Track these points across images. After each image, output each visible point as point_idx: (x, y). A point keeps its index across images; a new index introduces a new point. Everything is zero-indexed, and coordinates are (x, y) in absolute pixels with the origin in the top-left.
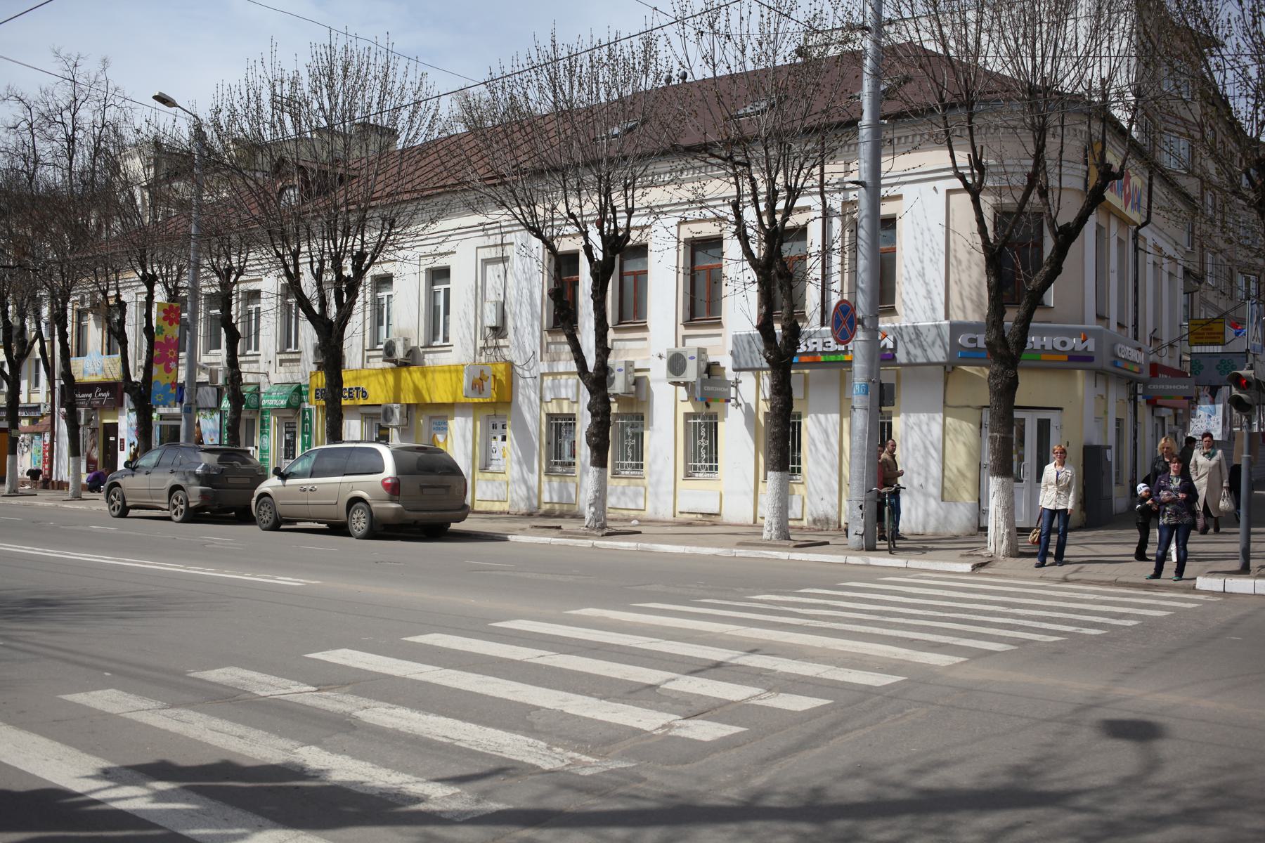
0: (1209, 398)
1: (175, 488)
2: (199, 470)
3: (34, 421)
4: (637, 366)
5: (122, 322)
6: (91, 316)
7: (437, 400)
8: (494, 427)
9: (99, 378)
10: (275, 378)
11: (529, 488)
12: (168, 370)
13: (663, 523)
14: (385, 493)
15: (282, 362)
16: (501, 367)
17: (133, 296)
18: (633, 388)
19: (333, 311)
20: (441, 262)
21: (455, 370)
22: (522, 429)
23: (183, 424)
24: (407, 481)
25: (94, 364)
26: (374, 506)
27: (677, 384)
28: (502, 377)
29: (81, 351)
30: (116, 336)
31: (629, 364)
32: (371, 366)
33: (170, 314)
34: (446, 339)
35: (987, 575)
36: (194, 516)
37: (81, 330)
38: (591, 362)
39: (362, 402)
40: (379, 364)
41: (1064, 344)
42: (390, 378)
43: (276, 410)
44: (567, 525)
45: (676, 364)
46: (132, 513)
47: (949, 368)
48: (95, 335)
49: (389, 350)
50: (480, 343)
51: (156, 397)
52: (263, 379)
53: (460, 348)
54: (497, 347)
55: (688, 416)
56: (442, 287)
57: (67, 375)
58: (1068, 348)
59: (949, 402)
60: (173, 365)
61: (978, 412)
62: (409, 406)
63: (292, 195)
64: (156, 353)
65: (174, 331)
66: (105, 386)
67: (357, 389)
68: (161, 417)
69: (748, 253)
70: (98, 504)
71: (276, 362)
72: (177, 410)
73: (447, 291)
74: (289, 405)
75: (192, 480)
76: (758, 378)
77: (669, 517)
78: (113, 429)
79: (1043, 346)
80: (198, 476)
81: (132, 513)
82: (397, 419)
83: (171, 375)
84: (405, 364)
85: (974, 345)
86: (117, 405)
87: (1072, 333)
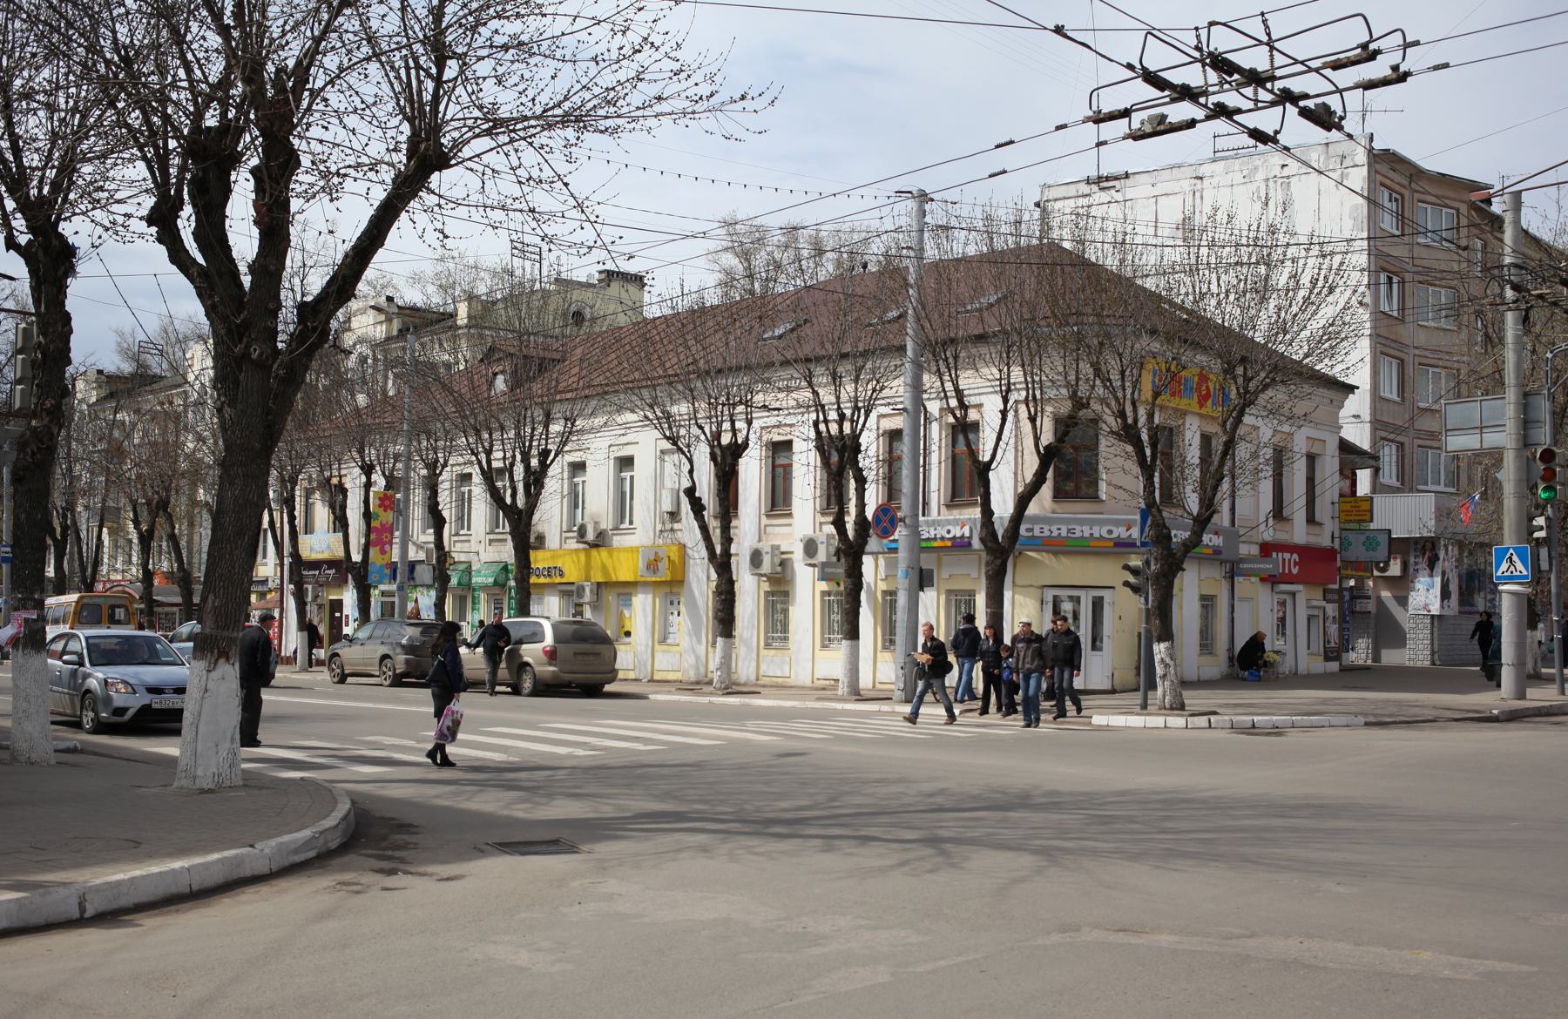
0: (1428, 571)
1: (385, 657)
2: (404, 641)
3: (262, 595)
4: (783, 549)
5: (344, 507)
6: (317, 495)
7: (622, 578)
9: (325, 556)
10: (485, 557)
11: (697, 658)
12: (383, 552)
13: (803, 688)
14: (545, 659)
15: (491, 541)
16: (675, 548)
17: (353, 479)
18: (779, 569)
19: (521, 502)
21: (634, 550)
22: (693, 605)
23: (396, 600)
24: (561, 648)
25: (320, 543)
26: (537, 669)
28: (674, 556)
29: (309, 529)
30: (340, 522)
31: (775, 548)
32: (565, 546)
33: (386, 501)
34: (631, 523)
36: (398, 681)
37: (308, 508)
38: (718, 549)
39: (558, 580)
40: (573, 544)
41: (1110, 532)
42: (582, 557)
43: (484, 588)
46: (349, 680)
48: (322, 514)
49: (582, 532)
50: (659, 527)
51: (372, 578)
52: (474, 558)
53: (641, 533)
54: (672, 530)
55: (824, 593)
57: (295, 554)
58: (1115, 535)
59: (1018, 582)
60: (387, 547)
62: (599, 584)
63: (500, 383)
64: (373, 536)
65: (388, 517)
66: (331, 563)
68: (383, 594)
70: (323, 676)
71: (481, 545)
72: (394, 587)
74: (496, 583)
75: (399, 650)
76: (876, 560)
77: (808, 683)
78: (337, 605)
80: (403, 647)
81: (349, 680)
82: (587, 597)
83: (386, 557)
84: (595, 545)
86: (341, 583)
87: (1117, 523)
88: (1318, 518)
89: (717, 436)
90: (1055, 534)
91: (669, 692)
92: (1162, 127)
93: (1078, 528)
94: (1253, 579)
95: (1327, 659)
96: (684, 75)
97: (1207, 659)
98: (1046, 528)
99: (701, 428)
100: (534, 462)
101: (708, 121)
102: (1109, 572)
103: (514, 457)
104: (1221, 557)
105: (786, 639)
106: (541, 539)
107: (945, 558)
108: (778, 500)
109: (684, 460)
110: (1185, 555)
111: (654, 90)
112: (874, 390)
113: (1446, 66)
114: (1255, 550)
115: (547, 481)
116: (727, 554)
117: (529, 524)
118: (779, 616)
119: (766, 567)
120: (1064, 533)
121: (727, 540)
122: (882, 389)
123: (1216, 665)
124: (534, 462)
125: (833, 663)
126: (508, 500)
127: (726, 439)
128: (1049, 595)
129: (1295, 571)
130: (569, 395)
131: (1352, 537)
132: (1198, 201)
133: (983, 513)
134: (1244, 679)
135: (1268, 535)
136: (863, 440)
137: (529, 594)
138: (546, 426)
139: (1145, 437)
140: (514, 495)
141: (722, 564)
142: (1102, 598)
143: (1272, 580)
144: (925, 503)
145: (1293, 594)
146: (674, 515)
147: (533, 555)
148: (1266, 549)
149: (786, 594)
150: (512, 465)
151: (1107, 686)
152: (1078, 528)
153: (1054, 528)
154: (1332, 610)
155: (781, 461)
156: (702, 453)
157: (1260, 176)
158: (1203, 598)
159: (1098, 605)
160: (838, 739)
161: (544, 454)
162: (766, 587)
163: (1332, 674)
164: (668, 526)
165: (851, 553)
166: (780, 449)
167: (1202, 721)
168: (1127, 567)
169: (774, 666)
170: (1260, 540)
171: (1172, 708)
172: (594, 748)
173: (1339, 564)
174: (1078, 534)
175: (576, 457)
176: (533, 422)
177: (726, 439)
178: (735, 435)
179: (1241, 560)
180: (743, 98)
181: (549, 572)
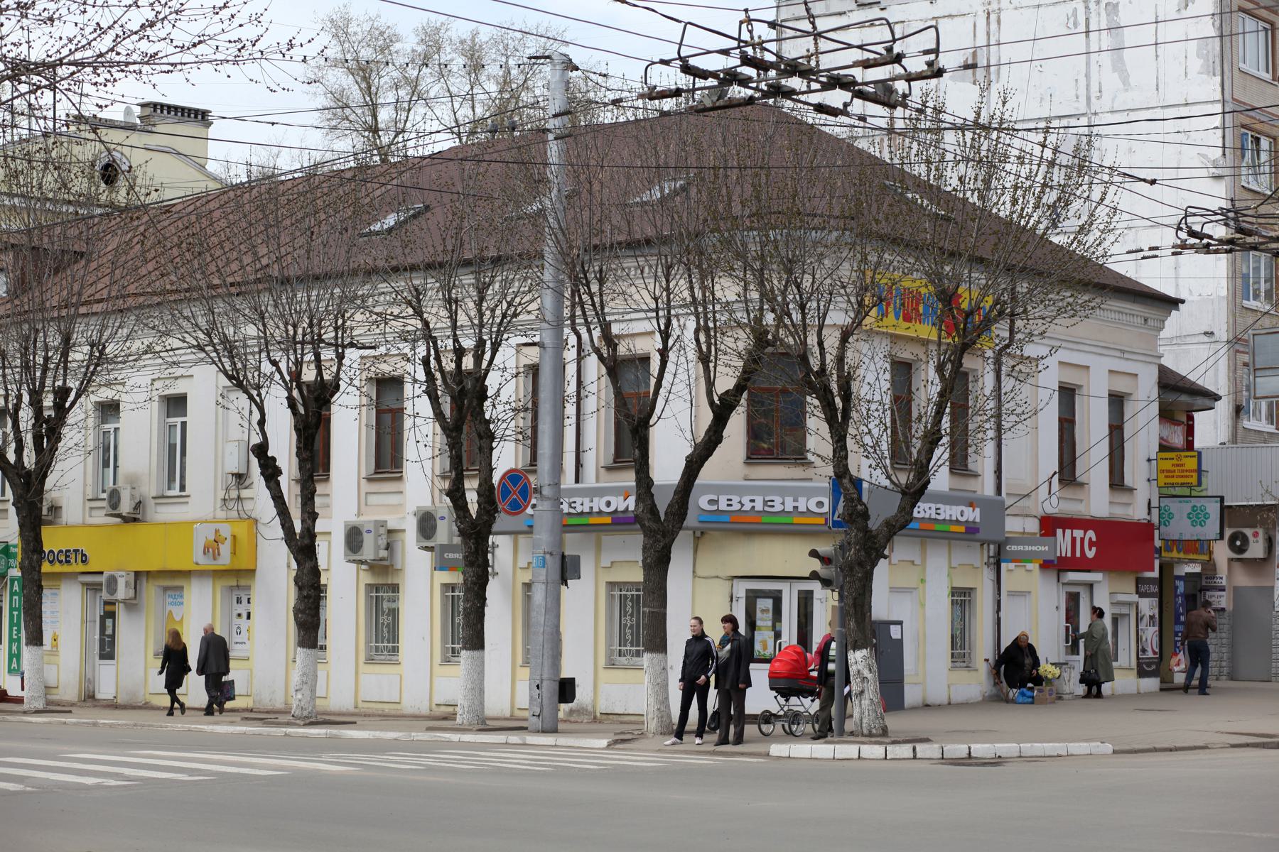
8: (239, 601)
18: (383, 554)
19: (29, 459)
20: (178, 388)
27: (426, 548)
34: (183, 488)
35: (639, 750)
38: (298, 527)
40: (100, 518)
44: (282, 718)
45: (354, 538)
47: (698, 534)
56: (179, 420)
59: (699, 572)
61: (728, 583)
67: (76, 551)
69: (439, 415)
73: (184, 424)
79: (796, 508)
85: (715, 508)
88: (1128, 481)
89: (296, 376)
90: (747, 507)
91: (232, 723)
92: (721, 103)
93: (778, 500)
94: (1029, 566)
95: (1142, 673)
96: (225, 14)
97: (962, 675)
98: (735, 499)
99: (274, 363)
100: (48, 401)
101: (251, 69)
102: (793, 558)
103: (19, 397)
104: (978, 536)
105: (395, 650)
106: (55, 509)
107: (606, 539)
108: (387, 459)
109: (254, 408)
110: (889, 538)
111: (196, 28)
112: (504, 316)
114: (1033, 526)
115: (65, 430)
116: (310, 534)
117: (40, 491)
118: (385, 620)
119: (368, 552)
120: (759, 506)
121: (310, 515)
122: (515, 315)
123: (977, 682)
124: (48, 401)
125: (451, 685)
126: (11, 457)
127: (309, 375)
128: (741, 589)
129: (1091, 554)
130: (97, 308)
131: (1174, 505)
132: (994, 26)
133: (638, 481)
134: (1013, 701)
135: (1054, 505)
136: (492, 381)
137: (40, 588)
138: (65, 355)
139: (834, 387)
140: (19, 451)
141: (304, 548)
143: (1056, 566)
144: (579, 464)
145: (1090, 586)
146: (240, 478)
147: (46, 532)
148: (1050, 525)
149: (395, 588)
150: (17, 407)
154: (1148, 606)
155: (390, 402)
156: (276, 400)
158: (955, 592)
160: (430, 770)
161: (62, 393)
162: (367, 578)
163: (1149, 695)
164: (234, 494)
165: (476, 536)
166: (388, 385)
167: (905, 751)
168: (814, 554)
169: (343, 672)
170: (1040, 513)
171: (870, 735)
172: (128, 778)
173: (1158, 543)
174: (778, 508)
175: (106, 394)
176: (46, 349)
177: (309, 375)
178: (319, 368)
179: (1008, 541)
180: (291, 45)
181: (66, 556)
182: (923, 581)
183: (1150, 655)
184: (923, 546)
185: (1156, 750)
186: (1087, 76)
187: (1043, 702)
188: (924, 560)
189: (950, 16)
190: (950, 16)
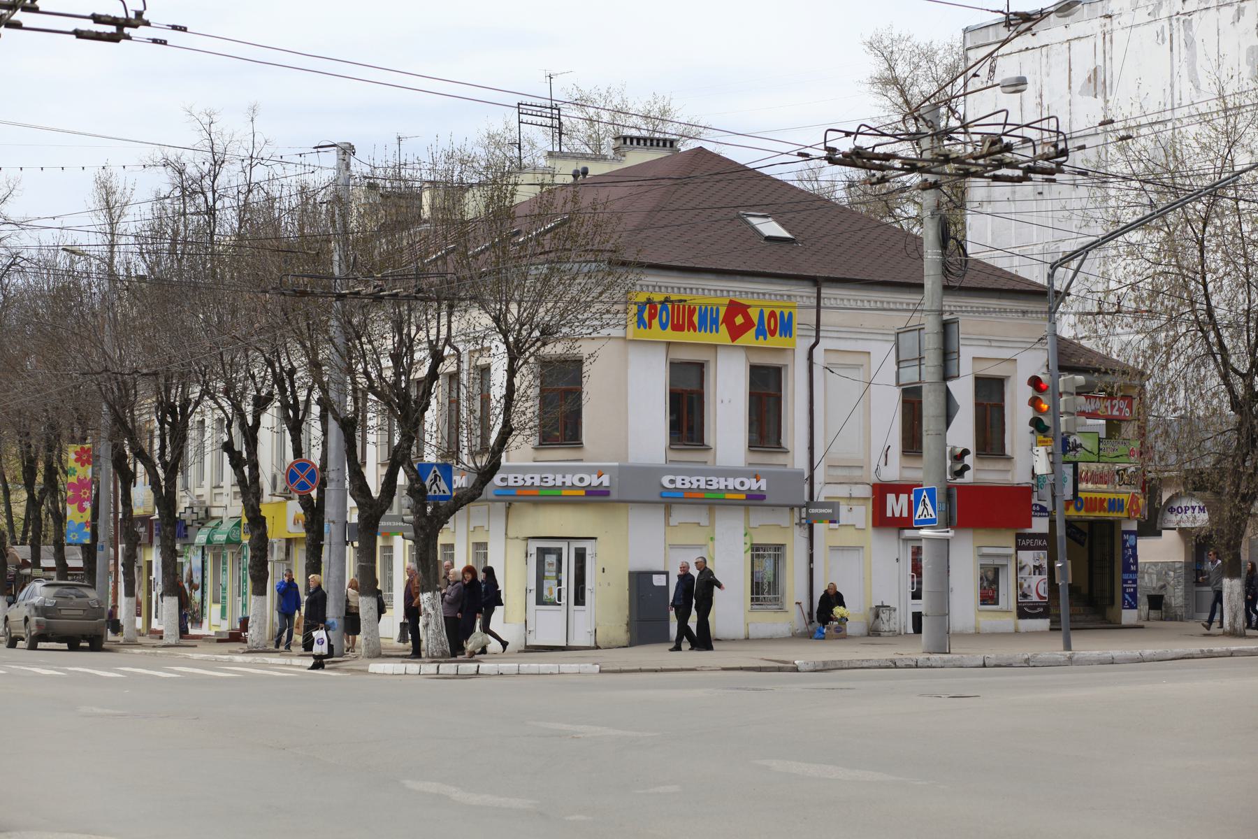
58: (586, 483)
59: (510, 535)
61: (524, 543)
63: (771, 228)
90: (528, 483)
93: (551, 477)
113: (185, 29)
128: (533, 547)
132: (1108, 44)
135: (893, 472)
142: (584, 549)
151: (589, 642)
152: (551, 477)
153: (527, 477)
157: (1164, 13)
159: (581, 556)
170: (874, 479)
174: (551, 483)
182: (712, 539)
183: (1035, 598)
184: (747, 512)
185: (641, 671)
186: (1172, 86)
187: (832, 638)
188: (712, 524)
189: (1079, 38)
190: (1079, 38)
